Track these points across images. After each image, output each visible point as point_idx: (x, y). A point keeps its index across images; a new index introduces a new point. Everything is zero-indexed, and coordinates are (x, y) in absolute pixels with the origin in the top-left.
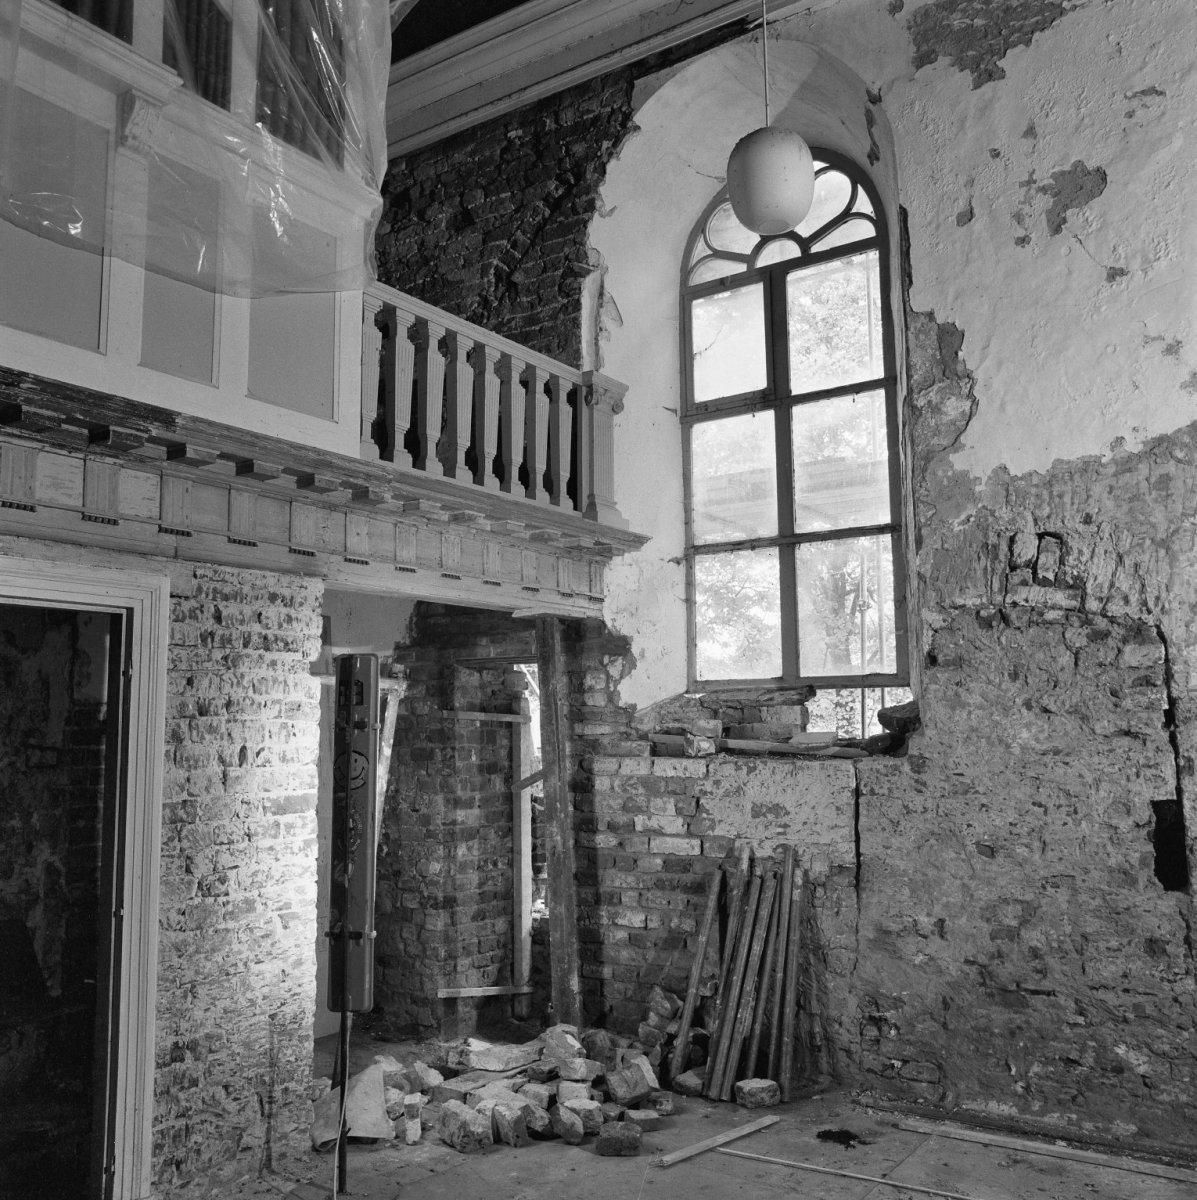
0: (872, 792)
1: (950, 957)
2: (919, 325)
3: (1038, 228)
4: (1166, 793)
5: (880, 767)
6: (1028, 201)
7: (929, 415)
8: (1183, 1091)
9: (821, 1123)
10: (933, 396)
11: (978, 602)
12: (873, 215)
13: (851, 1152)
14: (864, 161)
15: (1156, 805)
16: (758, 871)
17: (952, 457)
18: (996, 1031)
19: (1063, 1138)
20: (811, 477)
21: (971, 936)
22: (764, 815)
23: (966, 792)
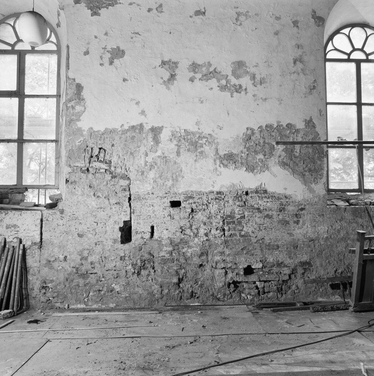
0: (47, 220)
1: (68, 267)
2: (70, 82)
3: (106, 60)
4: (127, 219)
5: (50, 213)
6: (104, 53)
7: (71, 109)
8: (127, 294)
9: (28, 319)
10: (72, 103)
11: (82, 165)
12: (56, 43)
13: (39, 325)
14: (55, 26)
15: (125, 222)
16: (7, 246)
17: (77, 123)
18: (81, 285)
19: (97, 311)
20: (30, 121)
21: (75, 259)
22: (10, 228)
23: (76, 220)
